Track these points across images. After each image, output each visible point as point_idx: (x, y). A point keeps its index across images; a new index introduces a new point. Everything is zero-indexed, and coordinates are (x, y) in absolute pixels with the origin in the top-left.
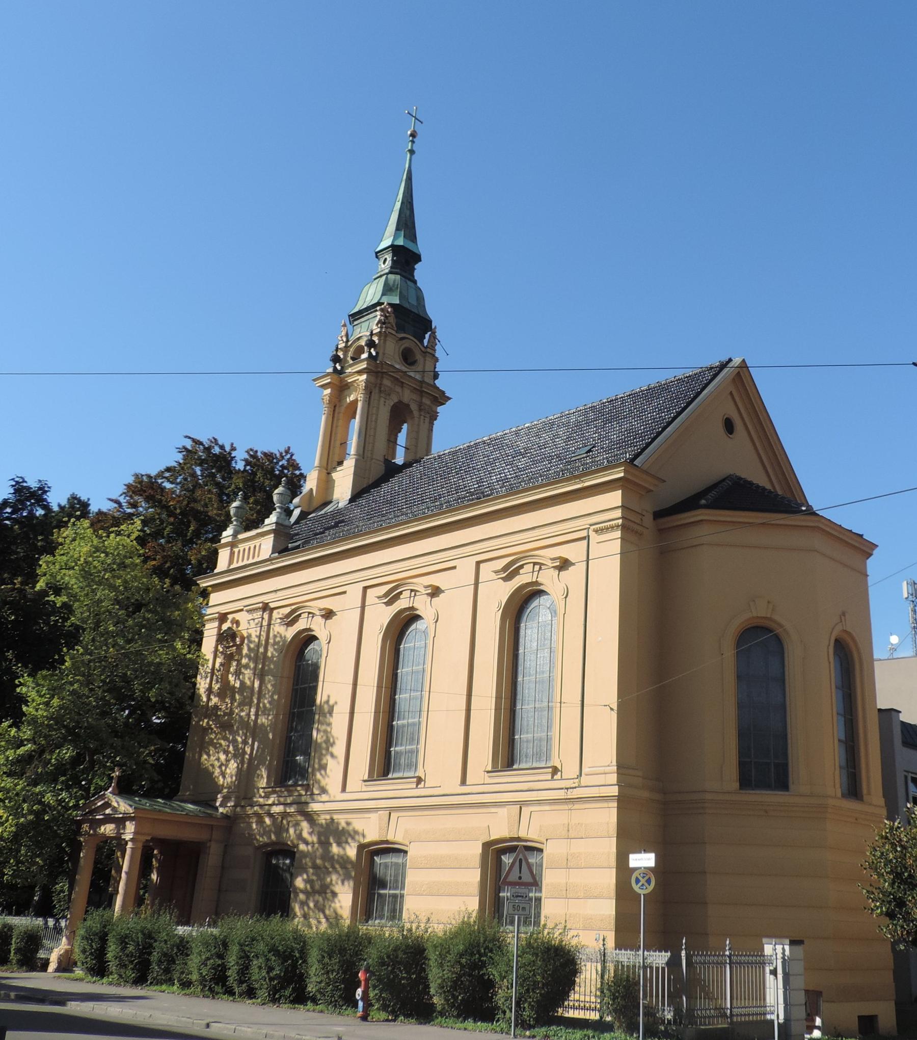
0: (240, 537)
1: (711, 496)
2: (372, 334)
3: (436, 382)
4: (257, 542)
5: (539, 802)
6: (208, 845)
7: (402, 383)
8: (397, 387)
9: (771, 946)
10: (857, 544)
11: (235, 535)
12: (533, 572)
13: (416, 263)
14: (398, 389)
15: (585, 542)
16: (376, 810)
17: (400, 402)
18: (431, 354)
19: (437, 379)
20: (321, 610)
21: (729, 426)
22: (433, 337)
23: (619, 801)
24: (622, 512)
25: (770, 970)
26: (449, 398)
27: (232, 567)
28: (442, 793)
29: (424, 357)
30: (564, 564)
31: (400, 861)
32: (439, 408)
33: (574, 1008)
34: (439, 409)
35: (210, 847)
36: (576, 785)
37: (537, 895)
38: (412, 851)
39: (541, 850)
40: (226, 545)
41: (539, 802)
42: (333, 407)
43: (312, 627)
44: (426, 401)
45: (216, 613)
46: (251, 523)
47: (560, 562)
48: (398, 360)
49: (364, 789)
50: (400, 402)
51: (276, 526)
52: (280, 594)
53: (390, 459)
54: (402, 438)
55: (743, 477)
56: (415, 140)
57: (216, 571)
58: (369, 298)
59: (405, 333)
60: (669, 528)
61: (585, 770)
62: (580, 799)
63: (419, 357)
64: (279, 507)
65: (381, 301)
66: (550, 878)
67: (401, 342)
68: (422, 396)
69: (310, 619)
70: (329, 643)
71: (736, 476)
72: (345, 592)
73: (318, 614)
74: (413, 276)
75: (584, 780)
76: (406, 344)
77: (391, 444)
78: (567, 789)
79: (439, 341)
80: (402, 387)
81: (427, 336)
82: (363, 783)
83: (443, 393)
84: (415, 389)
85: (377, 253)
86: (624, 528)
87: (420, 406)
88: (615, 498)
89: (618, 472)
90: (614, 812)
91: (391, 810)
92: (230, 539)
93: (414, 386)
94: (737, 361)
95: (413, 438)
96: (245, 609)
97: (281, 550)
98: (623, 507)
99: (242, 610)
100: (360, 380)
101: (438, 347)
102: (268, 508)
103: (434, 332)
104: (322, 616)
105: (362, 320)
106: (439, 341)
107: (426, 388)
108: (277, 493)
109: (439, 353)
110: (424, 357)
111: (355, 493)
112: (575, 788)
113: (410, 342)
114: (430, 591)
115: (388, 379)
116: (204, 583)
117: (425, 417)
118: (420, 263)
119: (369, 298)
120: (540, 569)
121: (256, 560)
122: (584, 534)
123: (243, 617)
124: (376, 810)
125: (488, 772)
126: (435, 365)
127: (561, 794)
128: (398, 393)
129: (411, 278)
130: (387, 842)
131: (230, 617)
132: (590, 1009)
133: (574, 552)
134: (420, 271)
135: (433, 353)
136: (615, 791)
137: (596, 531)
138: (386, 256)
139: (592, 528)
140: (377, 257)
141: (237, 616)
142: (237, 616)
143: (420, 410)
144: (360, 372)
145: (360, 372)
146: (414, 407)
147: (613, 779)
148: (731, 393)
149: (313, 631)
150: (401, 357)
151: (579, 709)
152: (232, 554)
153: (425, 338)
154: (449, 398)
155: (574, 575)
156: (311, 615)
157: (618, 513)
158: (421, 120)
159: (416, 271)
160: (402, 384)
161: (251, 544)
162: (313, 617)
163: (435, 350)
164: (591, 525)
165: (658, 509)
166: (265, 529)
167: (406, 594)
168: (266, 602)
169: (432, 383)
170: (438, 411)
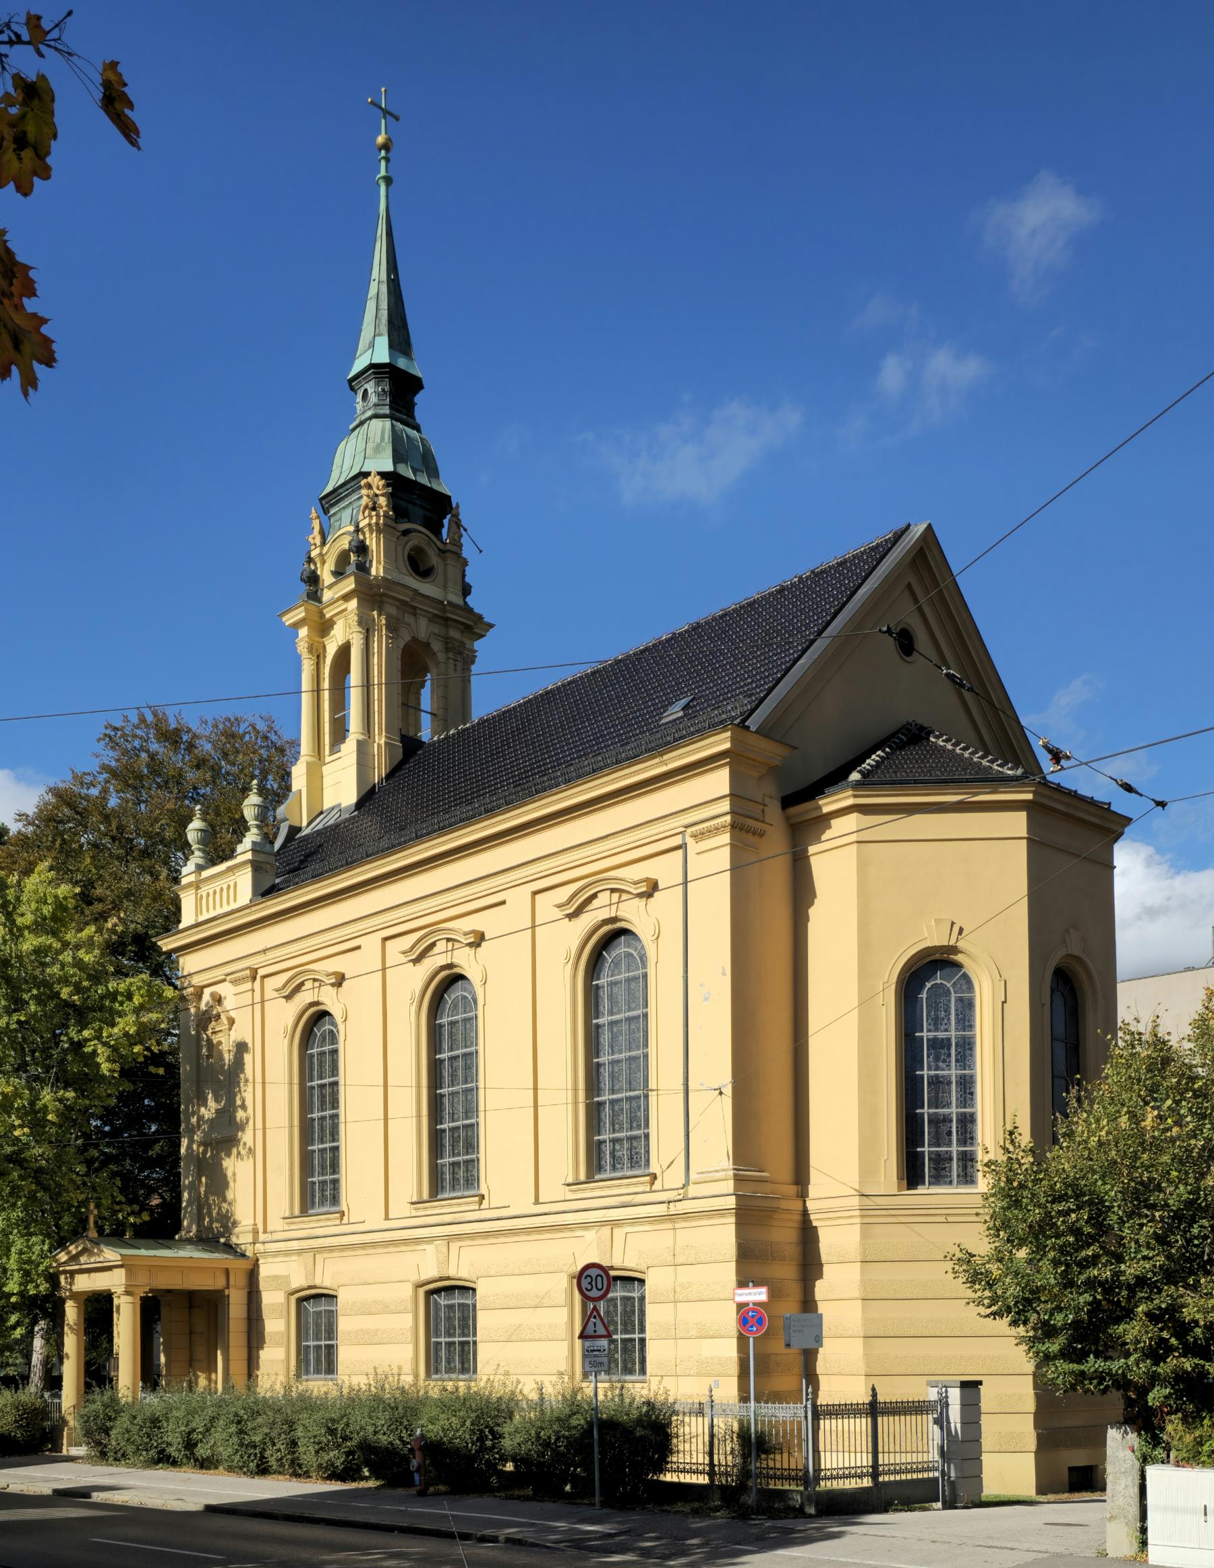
0: (205, 874)
1: (868, 764)
2: (358, 530)
3: (468, 599)
4: (229, 880)
5: (635, 1221)
6: (227, 1292)
7: (415, 608)
8: (406, 615)
9: (936, 1389)
10: (1097, 821)
11: (200, 868)
12: (263, 1002)
13: (416, 393)
14: (409, 619)
15: (680, 852)
16: (430, 1240)
17: (415, 640)
18: (456, 553)
19: (469, 594)
20: (328, 975)
21: (906, 643)
22: (457, 523)
23: (738, 1216)
24: (731, 804)
25: (934, 1419)
26: (491, 626)
27: (201, 919)
28: (367, 1229)
29: (444, 559)
30: (652, 888)
31: (469, 1302)
32: (476, 643)
33: (678, 1471)
34: (478, 645)
35: (228, 1296)
36: (681, 1197)
37: (641, 1336)
38: (343, 1297)
39: (642, 1281)
40: (189, 885)
41: (635, 1221)
42: (315, 658)
43: (321, 999)
44: (454, 634)
45: (247, 969)
46: (218, 852)
47: (475, 937)
48: (405, 571)
49: (414, 1213)
50: (415, 640)
51: (253, 855)
52: (271, 955)
53: (411, 734)
54: (426, 698)
55: (925, 725)
56: (390, 155)
57: (181, 926)
58: (346, 466)
59: (409, 522)
60: (814, 818)
61: (693, 1176)
62: (686, 1216)
63: (434, 560)
64: (199, 849)
65: (364, 470)
66: (654, 1315)
67: (406, 539)
68: (447, 626)
69: (316, 990)
70: (345, 1020)
71: (916, 725)
72: (359, 948)
73: (328, 982)
74: (413, 418)
75: (693, 1190)
76: (414, 540)
77: (412, 711)
78: (669, 1202)
79: (465, 530)
80: (415, 615)
81: (446, 522)
82: (567, 1188)
83: (480, 617)
84: (435, 615)
85: (351, 381)
86: (734, 826)
87: (447, 643)
88: (719, 782)
89: (722, 741)
90: (732, 1228)
91: (450, 1238)
92: (192, 878)
93: (436, 612)
94: (919, 529)
95: (443, 695)
96: (228, 978)
97: (264, 891)
98: (733, 795)
99: (224, 980)
100: (349, 609)
101: (465, 540)
102: (240, 827)
103: (456, 516)
104: (333, 985)
105: (342, 504)
106: (465, 530)
107: (452, 613)
108: (251, 805)
109: (467, 552)
110: (444, 559)
111: (364, 792)
112: (680, 1200)
113: (420, 536)
114: (334, 981)
115: (392, 605)
116: (166, 944)
117: (455, 661)
118: (421, 392)
119: (346, 466)
120: (320, 986)
121: (233, 906)
122: (677, 841)
123: (224, 989)
124: (430, 1240)
125: (569, 1185)
126: (464, 571)
127: (661, 1210)
128: (409, 625)
129: (410, 420)
130: (448, 1278)
131: (207, 992)
132: (696, 1472)
133: (666, 870)
134: (422, 410)
135: (457, 549)
136: (731, 1202)
137: (694, 836)
138: (367, 386)
139: (689, 830)
140: (352, 388)
141: (220, 989)
142: (220, 989)
143: (447, 650)
144: (346, 597)
145: (346, 597)
146: (436, 646)
147: (729, 1186)
148: (909, 586)
149: (322, 1004)
150: (407, 563)
151: (681, 1096)
152: (199, 900)
153: (443, 526)
154: (491, 626)
155: (667, 902)
156: (317, 984)
157: (725, 806)
158: (395, 113)
159: (416, 407)
160: (414, 611)
161: (223, 883)
162: (320, 986)
163: (460, 546)
164: (687, 827)
165: (789, 792)
166: (240, 859)
167: (441, 946)
168: (256, 967)
169: (462, 603)
170: (476, 648)
